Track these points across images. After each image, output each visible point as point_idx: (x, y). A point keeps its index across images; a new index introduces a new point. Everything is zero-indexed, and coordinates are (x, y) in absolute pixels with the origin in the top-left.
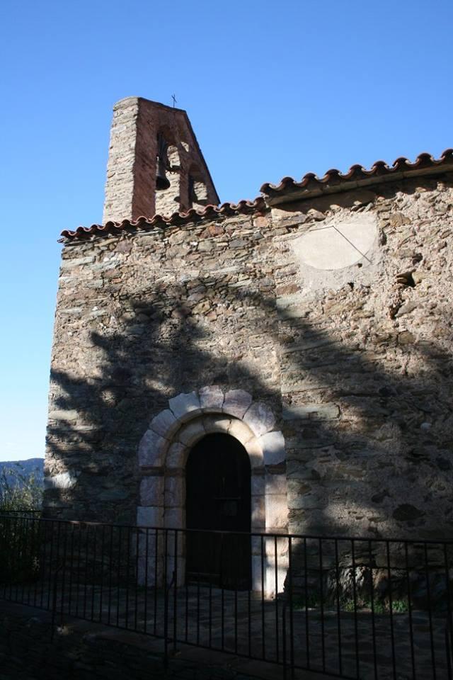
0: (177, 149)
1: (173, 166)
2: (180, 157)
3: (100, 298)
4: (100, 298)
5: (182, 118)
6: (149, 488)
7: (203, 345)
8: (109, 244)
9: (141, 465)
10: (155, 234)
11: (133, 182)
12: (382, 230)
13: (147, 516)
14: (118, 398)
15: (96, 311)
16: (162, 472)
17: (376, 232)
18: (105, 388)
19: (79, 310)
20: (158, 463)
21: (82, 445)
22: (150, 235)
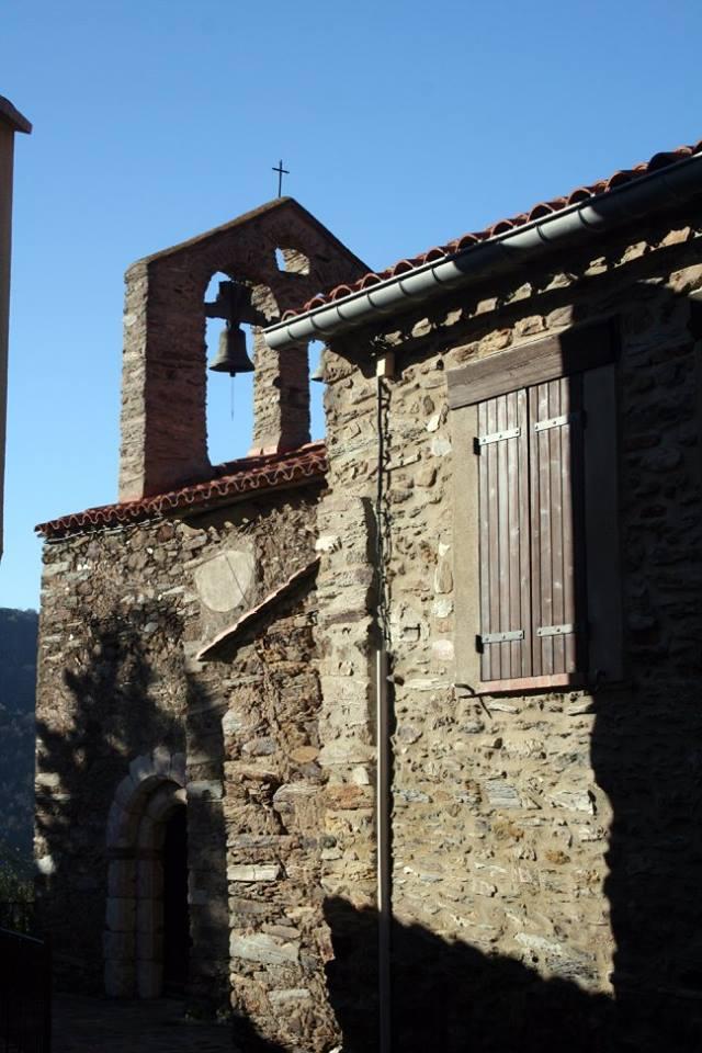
0: (269, 289)
1: (243, 334)
2: (278, 302)
3: (77, 623)
4: (77, 623)
5: (288, 215)
6: (116, 872)
7: (153, 692)
8: (81, 545)
9: (108, 845)
10: (119, 534)
11: (144, 415)
12: (258, 562)
13: (114, 909)
14: (89, 759)
15: (73, 641)
16: (129, 854)
17: (253, 564)
18: (79, 746)
19: (57, 638)
20: (122, 843)
21: (62, 820)
22: (115, 535)
